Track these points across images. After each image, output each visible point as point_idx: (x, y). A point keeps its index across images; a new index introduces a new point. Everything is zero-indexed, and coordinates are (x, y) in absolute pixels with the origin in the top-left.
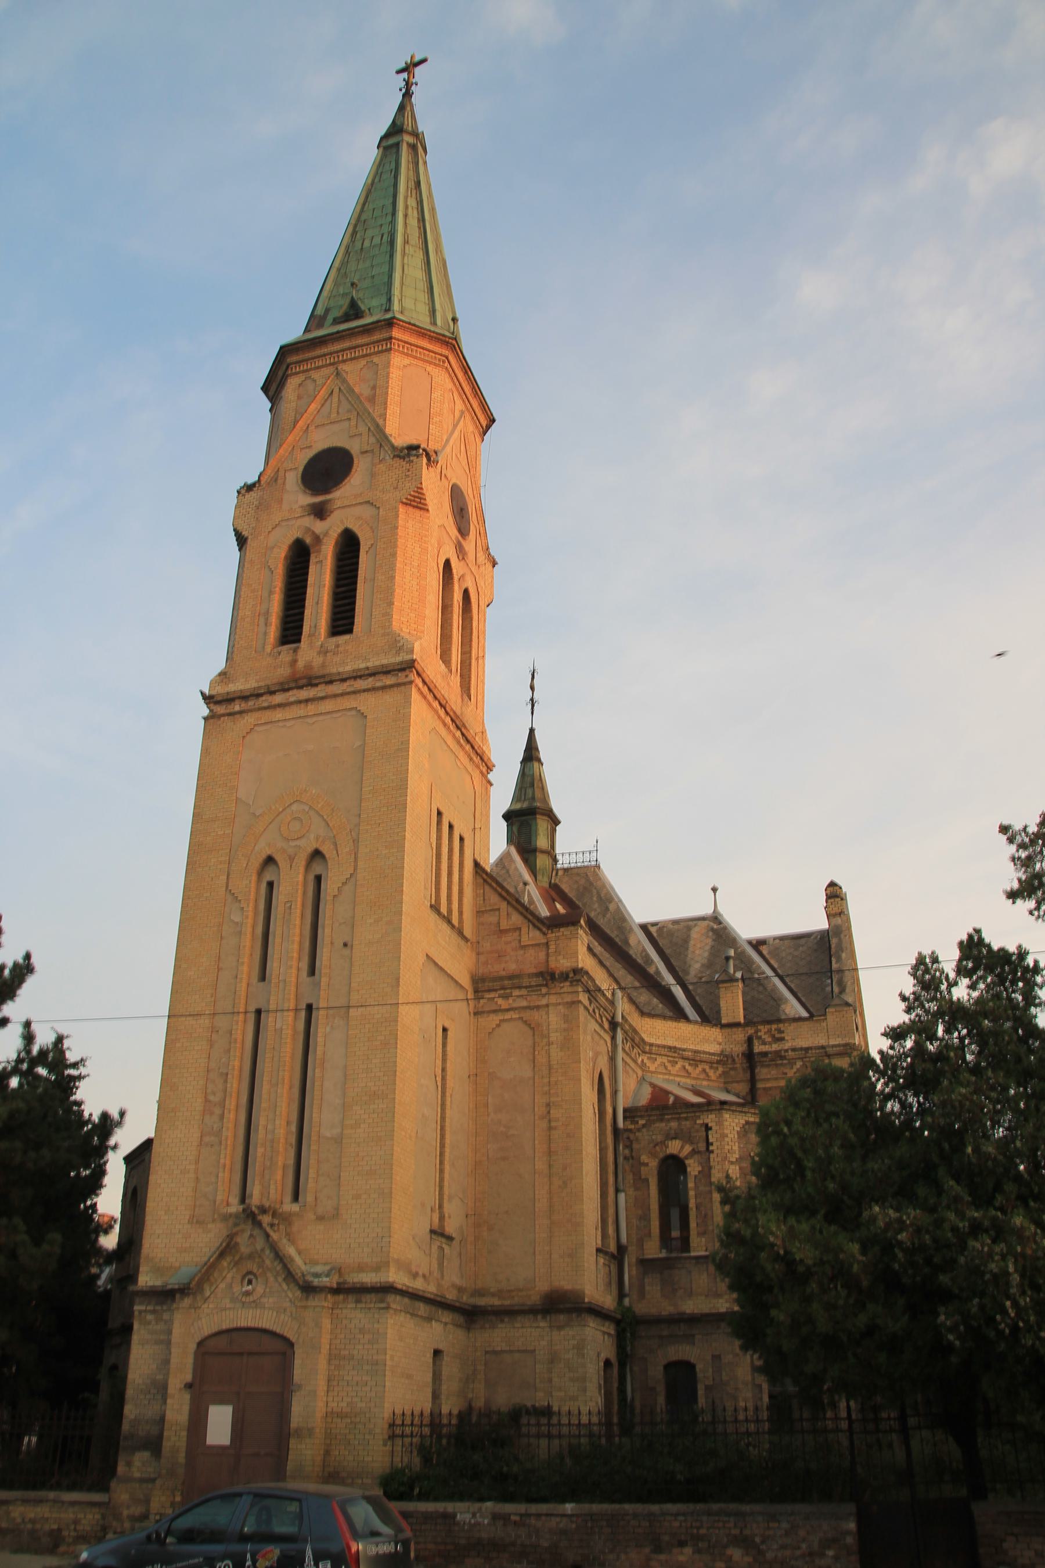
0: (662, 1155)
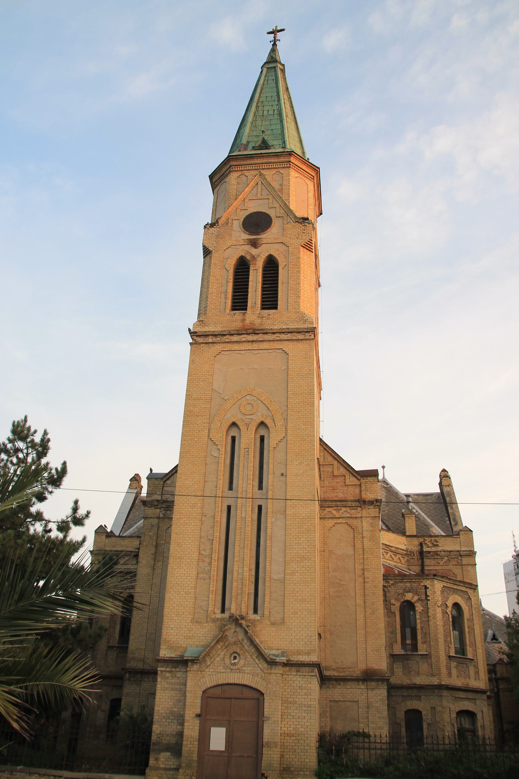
0: (402, 600)
